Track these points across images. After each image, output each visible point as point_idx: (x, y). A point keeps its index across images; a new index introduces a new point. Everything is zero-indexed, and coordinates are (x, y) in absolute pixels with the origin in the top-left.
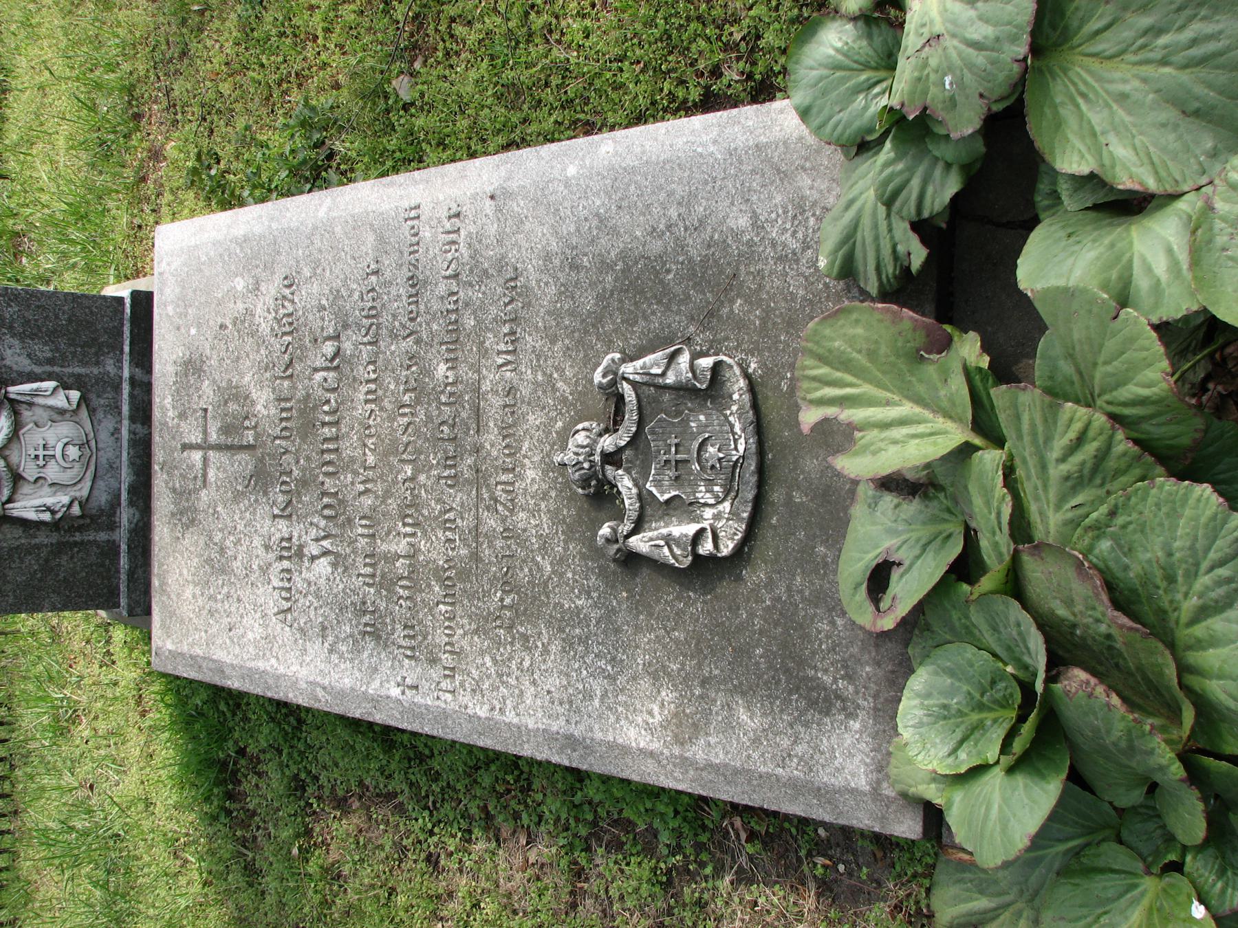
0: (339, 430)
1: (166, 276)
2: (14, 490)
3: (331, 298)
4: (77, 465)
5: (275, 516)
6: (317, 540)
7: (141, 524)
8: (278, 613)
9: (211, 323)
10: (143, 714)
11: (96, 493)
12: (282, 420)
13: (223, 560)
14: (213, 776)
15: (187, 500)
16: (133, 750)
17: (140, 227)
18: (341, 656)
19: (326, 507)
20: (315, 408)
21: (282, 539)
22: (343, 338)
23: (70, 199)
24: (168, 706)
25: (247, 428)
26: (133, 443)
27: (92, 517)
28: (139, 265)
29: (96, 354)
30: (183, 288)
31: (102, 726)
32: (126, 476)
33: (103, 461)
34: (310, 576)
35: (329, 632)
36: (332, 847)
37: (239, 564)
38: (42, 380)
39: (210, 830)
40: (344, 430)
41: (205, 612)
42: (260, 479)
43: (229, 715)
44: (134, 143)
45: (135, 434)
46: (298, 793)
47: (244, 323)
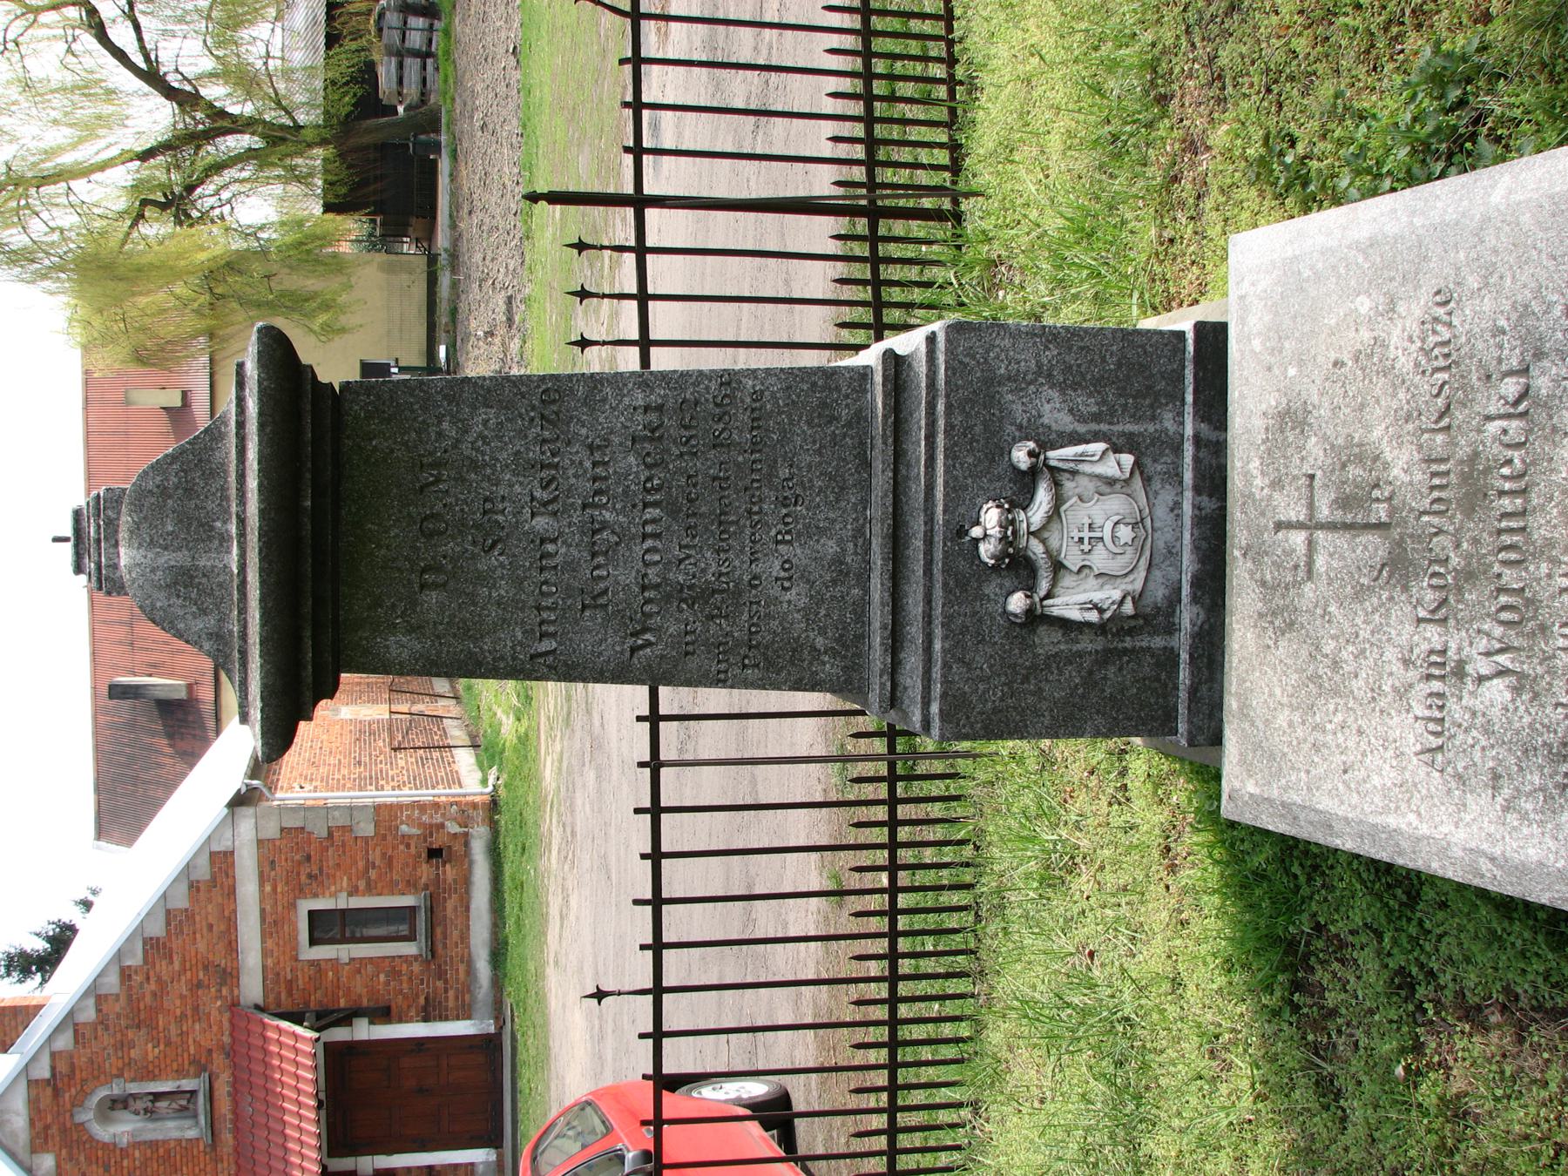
0: (1527, 501)
1: (1249, 299)
2: (1054, 582)
3: (1514, 316)
4: (1130, 550)
5: (1420, 621)
6: (1488, 654)
7: (1206, 627)
8: (1422, 752)
9: (1320, 359)
10: (1173, 869)
11: (1151, 586)
12: (1433, 488)
13: (1337, 678)
14: (1276, 958)
15: (1283, 596)
16: (1157, 914)
17: (1171, 241)
18: (1524, 816)
19: (1504, 608)
20: (1487, 471)
21: (1432, 652)
22: (1534, 372)
23: (1069, 213)
24: (1216, 862)
25: (1378, 500)
26: (1198, 521)
27: (1145, 617)
28: (1172, 290)
29: (1151, 406)
30: (1276, 314)
31: (1110, 879)
32: (1188, 564)
33: (1161, 544)
34: (1477, 704)
35: (1504, 781)
36: (1455, 1072)
37: (1361, 683)
38: (1087, 442)
39: (1269, 1029)
40: (1535, 502)
41: (1306, 747)
42: (1397, 569)
43: (1302, 879)
44: (1162, 133)
45: (1200, 509)
46: (1403, 993)
47: (1372, 359)
